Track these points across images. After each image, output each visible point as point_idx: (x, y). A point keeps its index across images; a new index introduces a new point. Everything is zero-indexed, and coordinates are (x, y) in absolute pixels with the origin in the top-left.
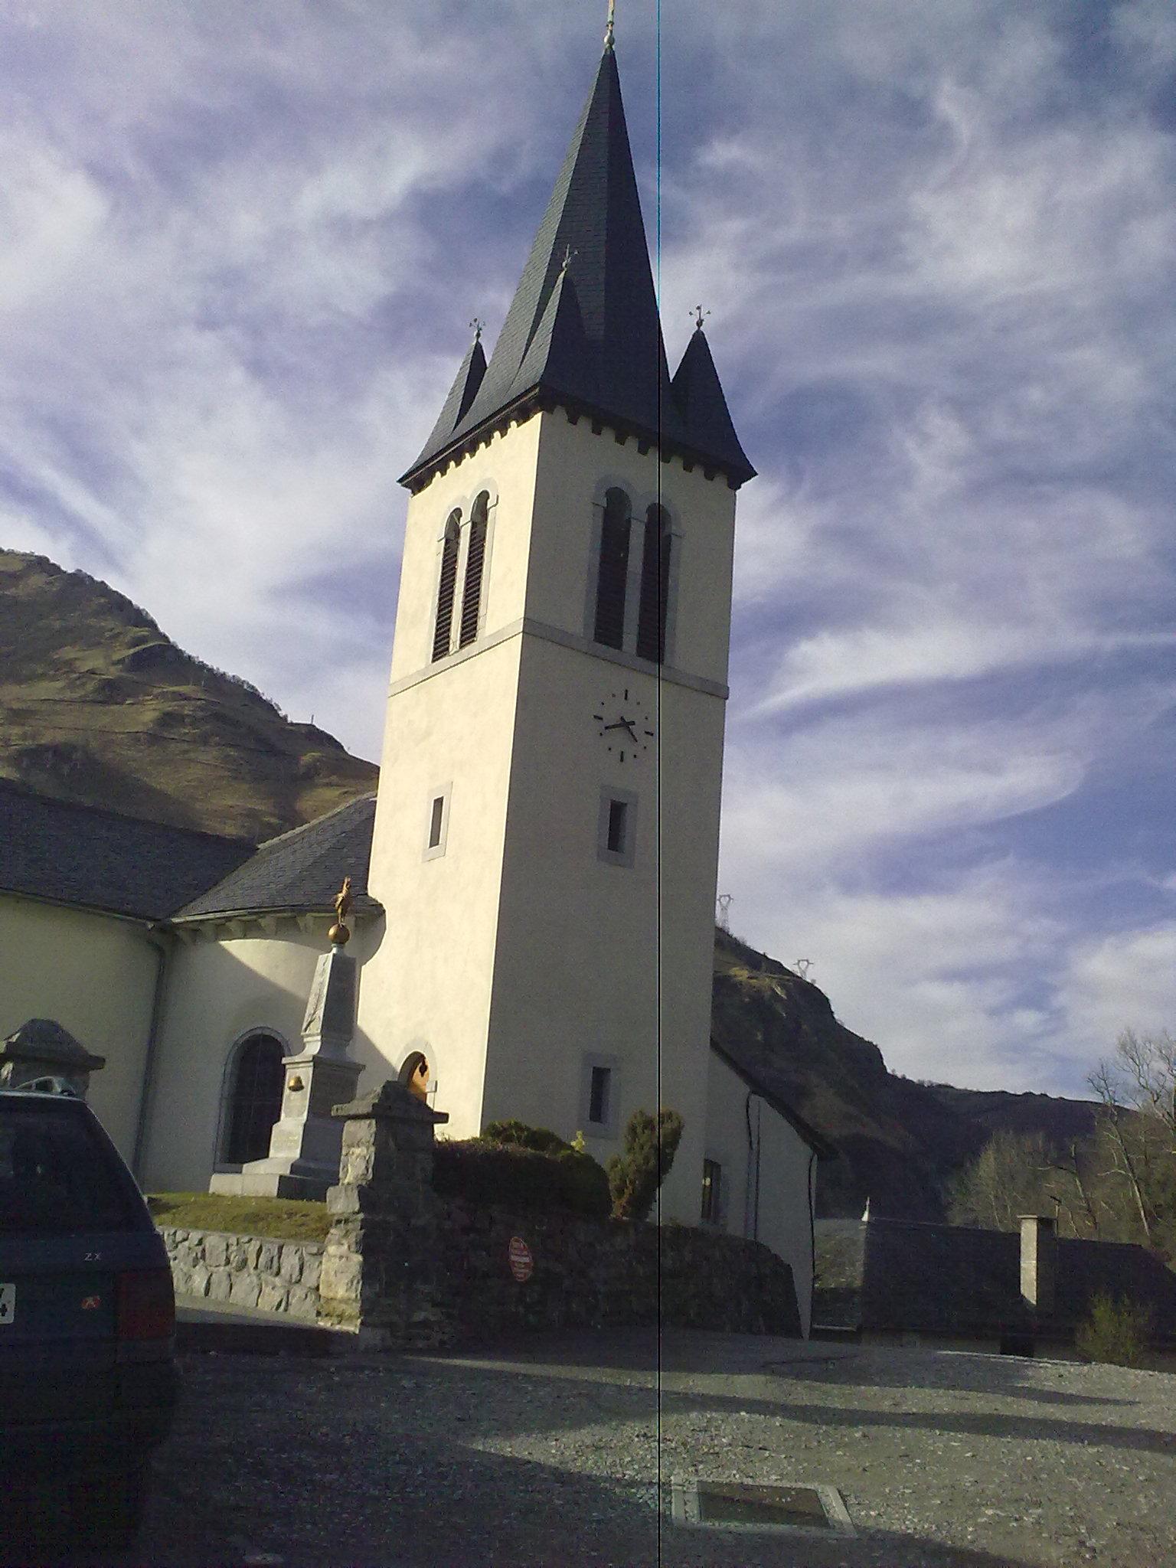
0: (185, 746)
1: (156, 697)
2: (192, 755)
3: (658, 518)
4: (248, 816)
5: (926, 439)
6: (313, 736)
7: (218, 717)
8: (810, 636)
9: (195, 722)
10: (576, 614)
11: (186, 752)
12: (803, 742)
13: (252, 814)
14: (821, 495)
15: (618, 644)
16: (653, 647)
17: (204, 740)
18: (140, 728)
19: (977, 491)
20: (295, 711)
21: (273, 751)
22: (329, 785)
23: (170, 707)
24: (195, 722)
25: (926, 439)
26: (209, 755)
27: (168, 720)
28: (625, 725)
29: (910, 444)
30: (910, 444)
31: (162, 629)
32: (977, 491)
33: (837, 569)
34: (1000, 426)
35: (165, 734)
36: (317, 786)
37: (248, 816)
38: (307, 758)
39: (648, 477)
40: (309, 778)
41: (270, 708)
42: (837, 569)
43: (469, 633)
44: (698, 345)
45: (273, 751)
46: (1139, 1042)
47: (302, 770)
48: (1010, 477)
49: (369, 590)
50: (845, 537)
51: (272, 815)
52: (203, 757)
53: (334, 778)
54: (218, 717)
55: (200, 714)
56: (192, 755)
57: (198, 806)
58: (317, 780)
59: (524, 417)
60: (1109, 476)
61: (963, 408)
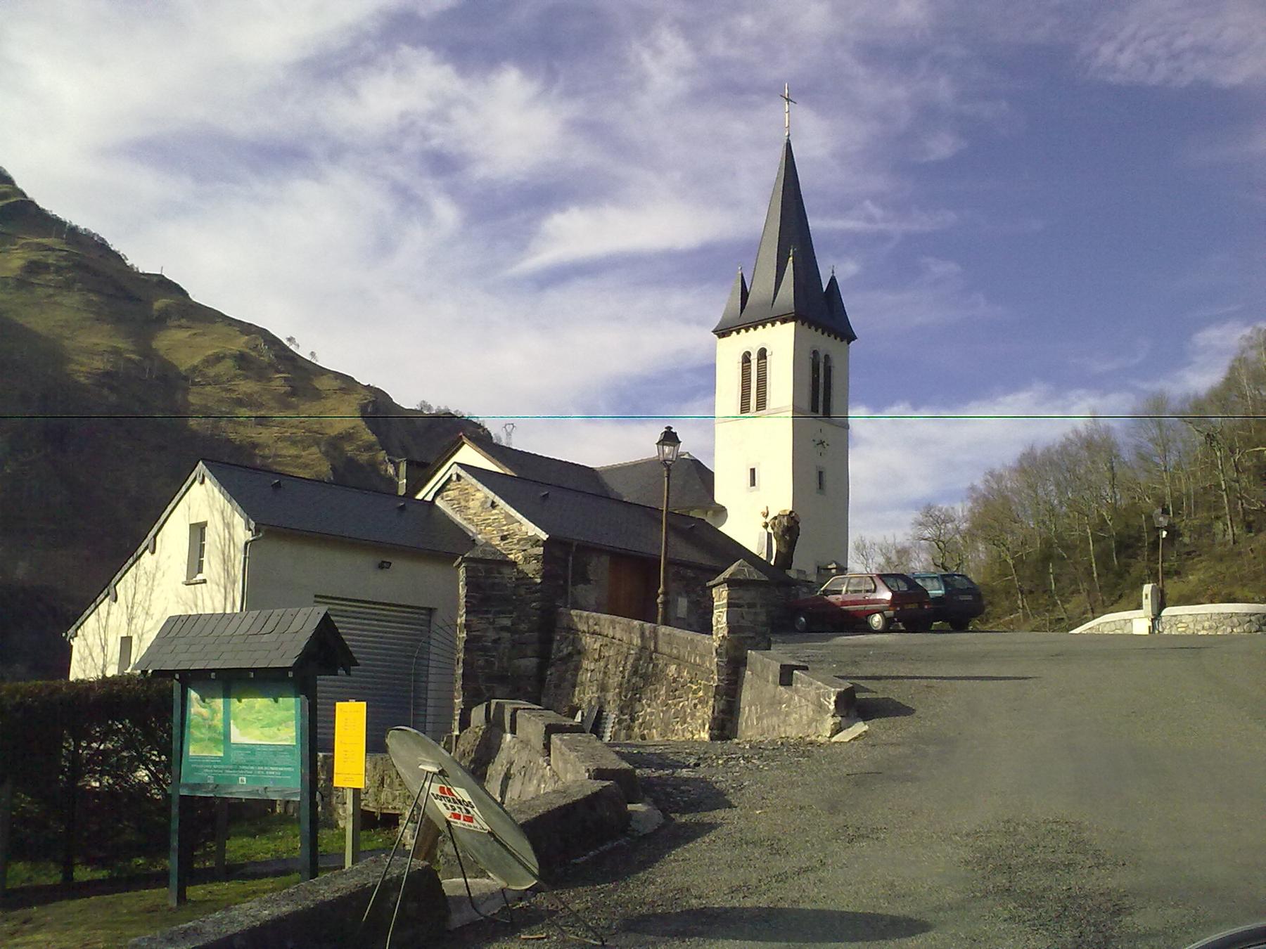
0: (51, 291)
1: (22, 246)
2: (58, 299)
3: (827, 357)
4: (111, 353)
5: (658, 53)
6: (163, 285)
7: (79, 266)
8: (563, 210)
9: (59, 270)
10: (806, 405)
11: (51, 296)
12: (555, 298)
13: (116, 352)
14: (571, 93)
15: (817, 412)
16: (827, 413)
17: (68, 286)
18: (9, 274)
19: (698, 97)
20: (143, 260)
21: (130, 298)
22: (180, 327)
23: (35, 256)
24: (59, 270)
25: (658, 53)
26: (72, 299)
27: (34, 268)
28: (822, 443)
29: (646, 56)
30: (646, 56)
31: (19, 185)
32: (698, 97)
33: (583, 155)
34: (719, 47)
35: (33, 280)
36: (168, 328)
37: (111, 353)
38: (159, 304)
39: (826, 344)
40: (161, 321)
41: (118, 258)
42: (583, 155)
43: (761, 404)
44: (833, 280)
45: (130, 298)
46: (868, 545)
47: (156, 314)
48: (726, 88)
49: (702, 378)
50: (590, 129)
51: (133, 352)
52: (67, 301)
53: (183, 321)
54: (79, 266)
55: (64, 264)
56: (58, 299)
57: (66, 343)
58: (169, 323)
59: (784, 321)
60: (800, 92)
61: (689, 30)
